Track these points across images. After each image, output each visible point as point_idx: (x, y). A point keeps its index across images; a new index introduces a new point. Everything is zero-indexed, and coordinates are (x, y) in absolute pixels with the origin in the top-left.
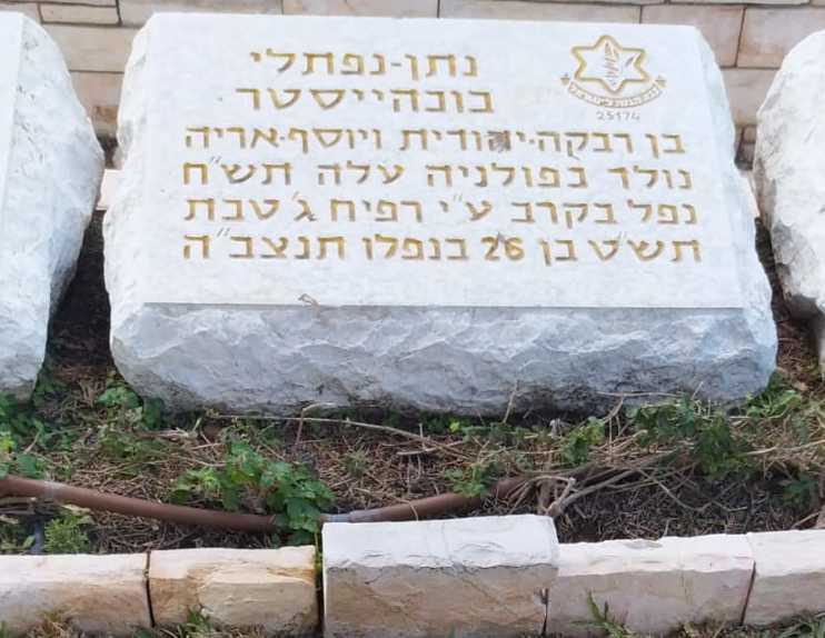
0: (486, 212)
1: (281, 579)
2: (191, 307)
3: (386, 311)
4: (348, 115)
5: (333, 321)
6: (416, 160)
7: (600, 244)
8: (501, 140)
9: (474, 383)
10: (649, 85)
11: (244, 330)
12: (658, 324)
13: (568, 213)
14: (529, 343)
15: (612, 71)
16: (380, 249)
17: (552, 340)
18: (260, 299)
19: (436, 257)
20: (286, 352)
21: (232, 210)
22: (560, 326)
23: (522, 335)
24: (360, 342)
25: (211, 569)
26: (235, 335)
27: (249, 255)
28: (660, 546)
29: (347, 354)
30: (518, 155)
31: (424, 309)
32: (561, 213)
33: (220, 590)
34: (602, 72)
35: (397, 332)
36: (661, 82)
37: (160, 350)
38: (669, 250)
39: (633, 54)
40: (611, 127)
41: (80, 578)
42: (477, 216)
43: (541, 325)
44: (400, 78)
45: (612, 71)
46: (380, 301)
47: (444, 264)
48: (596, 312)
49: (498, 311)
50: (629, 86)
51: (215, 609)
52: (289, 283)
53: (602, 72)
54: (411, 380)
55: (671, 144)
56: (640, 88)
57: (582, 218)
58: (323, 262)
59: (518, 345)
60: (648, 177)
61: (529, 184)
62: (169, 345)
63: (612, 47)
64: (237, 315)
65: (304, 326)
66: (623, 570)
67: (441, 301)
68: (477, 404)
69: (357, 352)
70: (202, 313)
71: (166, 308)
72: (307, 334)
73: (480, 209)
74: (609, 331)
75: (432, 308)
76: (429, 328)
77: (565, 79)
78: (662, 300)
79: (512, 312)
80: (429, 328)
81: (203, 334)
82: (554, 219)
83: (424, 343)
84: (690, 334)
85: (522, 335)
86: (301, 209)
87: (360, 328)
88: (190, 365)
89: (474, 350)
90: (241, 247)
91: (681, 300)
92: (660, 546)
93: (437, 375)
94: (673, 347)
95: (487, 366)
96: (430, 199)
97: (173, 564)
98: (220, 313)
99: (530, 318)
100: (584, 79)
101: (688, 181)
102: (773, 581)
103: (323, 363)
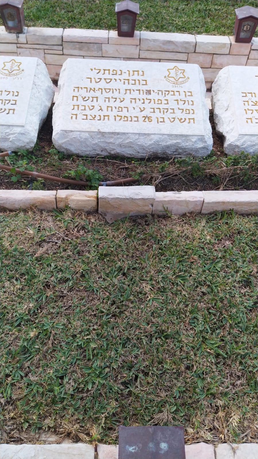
1: (88, 199)
2: (72, 131)
3: (118, 134)
4: (113, 85)
6: (128, 96)
8: (149, 92)
9: (139, 151)
11: (84, 137)
14: (152, 142)
23: (151, 140)
24: (112, 140)
25: (72, 195)
26: (82, 138)
29: (109, 143)
30: (153, 96)
31: (127, 133)
33: (73, 200)
34: (174, 75)
35: (121, 138)
42: (142, 111)
43: (155, 138)
44: (125, 76)
46: (117, 131)
48: (170, 135)
49: (145, 134)
50: (173, 78)
51: (72, 205)
53: (174, 75)
56: (17, 72)
59: (150, 143)
63: (177, 69)
64: (83, 133)
66: (171, 199)
67: (132, 131)
69: (111, 143)
71: (66, 131)
72: (99, 138)
74: (172, 140)
78: (185, 133)
79: (148, 135)
80: (128, 138)
81: (74, 138)
84: (191, 141)
86: (100, 108)
88: (71, 145)
90: (85, 117)
94: (187, 144)
95: (142, 147)
97: (63, 193)
98: (78, 133)
99: (153, 136)
102: (208, 203)
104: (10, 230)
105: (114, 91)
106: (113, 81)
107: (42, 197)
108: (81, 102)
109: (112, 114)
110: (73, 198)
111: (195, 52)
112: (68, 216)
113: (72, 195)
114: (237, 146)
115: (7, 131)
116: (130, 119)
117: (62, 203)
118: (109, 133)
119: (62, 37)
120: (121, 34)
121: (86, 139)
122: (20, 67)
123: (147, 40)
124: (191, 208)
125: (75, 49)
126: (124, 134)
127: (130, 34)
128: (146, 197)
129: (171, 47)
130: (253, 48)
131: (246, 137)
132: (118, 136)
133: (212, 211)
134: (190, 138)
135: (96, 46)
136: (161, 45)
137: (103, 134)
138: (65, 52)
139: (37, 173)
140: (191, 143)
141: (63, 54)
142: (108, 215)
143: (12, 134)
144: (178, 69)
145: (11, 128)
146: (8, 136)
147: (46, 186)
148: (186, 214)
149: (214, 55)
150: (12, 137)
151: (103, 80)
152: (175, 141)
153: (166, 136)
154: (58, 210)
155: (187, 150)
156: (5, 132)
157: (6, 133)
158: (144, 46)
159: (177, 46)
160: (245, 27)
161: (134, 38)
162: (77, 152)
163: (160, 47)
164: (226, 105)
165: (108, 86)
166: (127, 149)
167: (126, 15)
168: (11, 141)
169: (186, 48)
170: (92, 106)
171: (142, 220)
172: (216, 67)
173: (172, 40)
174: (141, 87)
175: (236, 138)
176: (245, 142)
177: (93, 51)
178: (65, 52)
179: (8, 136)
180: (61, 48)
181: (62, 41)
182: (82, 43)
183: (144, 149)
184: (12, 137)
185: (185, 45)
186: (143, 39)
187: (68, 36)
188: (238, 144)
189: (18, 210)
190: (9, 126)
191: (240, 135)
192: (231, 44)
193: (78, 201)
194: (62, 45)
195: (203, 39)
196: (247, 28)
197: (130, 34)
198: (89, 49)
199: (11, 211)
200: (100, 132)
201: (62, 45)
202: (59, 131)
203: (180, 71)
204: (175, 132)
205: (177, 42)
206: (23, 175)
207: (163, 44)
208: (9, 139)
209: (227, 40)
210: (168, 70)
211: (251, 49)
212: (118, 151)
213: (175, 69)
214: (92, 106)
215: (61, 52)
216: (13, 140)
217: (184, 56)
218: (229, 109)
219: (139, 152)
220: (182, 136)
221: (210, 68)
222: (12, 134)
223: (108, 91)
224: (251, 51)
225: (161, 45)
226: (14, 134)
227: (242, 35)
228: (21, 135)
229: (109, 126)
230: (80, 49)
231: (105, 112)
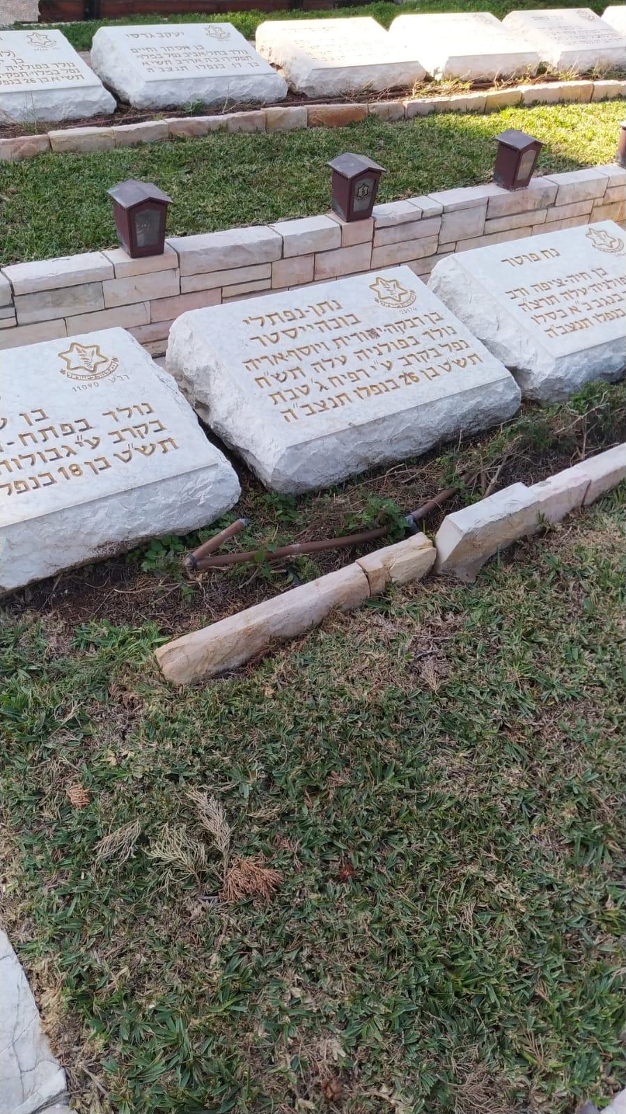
0: (98, 443)
1: (423, 551)
2: (306, 443)
3: (384, 419)
4: (304, 339)
5: (365, 430)
6: (348, 351)
7: (121, 455)
8: (373, 333)
9: (422, 440)
10: (109, 363)
11: (331, 447)
12: (483, 393)
14: (442, 414)
15: (86, 361)
16: (363, 393)
17: (450, 411)
18: (333, 430)
19: (37, 487)
20: (347, 451)
21: (290, 395)
22: (451, 404)
23: (438, 413)
24: (375, 437)
25: (390, 558)
26: (328, 450)
27: (314, 412)
28: (550, 482)
29: (369, 444)
30: (384, 337)
31: (398, 413)
32: (13, 465)
33: (400, 566)
35: (389, 427)
36: (115, 359)
37: (296, 468)
38: (159, 448)
39: (92, 349)
40: (410, 316)
41: (341, 584)
42: (389, 368)
43: (445, 406)
44: (312, 318)
45: (86, 361)
46: (381, 415)
47: (42, 490)
48: (463, 394)
49: (426, 405)
51: (399, 577)
52: (341, 418)
54: (396, 447)
55: (38, 415)
57: (146, 432)
58: (345, 406)
59: (438, 417)
60: (127, 412)
61: (57, 436)
62: (299, 464)
64: (327, 441)
65: (353, 437)
66: (549, 496)
67: (403, 408)
68: (204, 524)
69: (375, 442)
70: (312, 444)
71: (296, 447)
72: (355, 440)
73: (95, 442)
74: (467, 401)
75: (402, 412)
76: (402, 421)
78: (482, 382)
79: (431, 404)
80: (402, 421)
81: (314, 454)
83: (402, 429)
84: (496, 392)
85: (438, 413)
86: (319, 386)
87: (375, 430)
88: (307, 471)
89: (422, 425)
90: (308, 410)
91: (488, 380)
92: (550, 482)
93: (406, 441)
94: (492, 400)
95: (427, 431)
96: (366, 364)
97: (374, 560)
98: (319, 442)
99: (439, 404)
101: (149, 408)
102: (598, 481)
103: (362, 452)
104: (339, 671)
105: (317, 347)
106: (300, 331)
107: (347, 583)
108: (276, 386)
109: (348, 387)
110: (397, 561)
111: (282, 258)
112: (399, 602)
113: (390, 558)
114: (560, 380)
115: (189, 485)
117: (380, 580)
118: (370, 423)
119: (12, 286)
120: (136, 253)
121: (335, 449)
122: (101, 352)
123: (192, 253)
124: (575, 501)
125: (45, 306)
126: (393, 415)
127: (156, 249)
128: (529, 504)
129: (239, 259)
130: (377, 226)
131: (567, 360)
132: (385, 424)
133: (597, 495)
134: (493, 387)
135: (90, 290)
136: (222, 258)
137: (357, 429)
138: (22, 318)
139: (421, 510)
140: (497, 397)
141: (17, 325)
142: (457, 571)
143: (201, 489)
145: (193, 476)
146: (192, 496)
147: (329, 563)
148: (568, 515)
149: (317, 255)
150: (202, 497)
151: (282, 336)
152: (473, 402)
153: (458, 397)
154: (378, 598)
155: (492, 412)
156: (185, 489)
157: (188, 491)
158: (188, 267)
159: (250, 252)
160: (360, 190)
161: (164, 255)
162: (319, 483)
163: (220, 262)
164: (494, 321)
165: (299, 343)
166: (401, 444)
167: (147, 211)
168: (202, 506)
169: (266, 253)
171: (522, 548)
172: (324, 276)
173: (240, 243)
174: (353, 329)
175: (554, 367)
176: (568, 368)
177: (86, 301)
178: (22, 318)
179: (192, 496)
180: (11, 311)
181: (13, 295)
182: (57, 289)
183: (429, 434)
184: (202, 497)
185: (265, 248)
186: (184, 253)
187: (26, 280)
188: (560, 374)
189: (308, 631)
190: (188, 474)
191: (557, 359)
192: (341, 227)
193: (409, 562)
194: (13, 305)
195: (286, 228)
196: (363, 192)
197: (156, 249)
198: (76, 299)
199: (297, 638)
200: (355, 427)
201: (13, 305)
202: (283, 452)
204: (467, 386)
205: (249, 245)
206: (272, 560)
207: (225, 255)
208: (198, 500)
209: (326, 222)
211: (375, 229)
212: (387, 454)
215: (13, 322)
216: (208, 499)
217: (452, 247)
218: (501, 325)
219: (420, 443)
220: (481, 388)
221: (314, 281)
222: (201, 489)
223: (306, 351)
224: (377, 232)
225: (222, 258)
226: (206, 486)
227: (357, 205)
228: (218, 485)
229: (363, 411)
230: (57, 304)
231: (333, 392)
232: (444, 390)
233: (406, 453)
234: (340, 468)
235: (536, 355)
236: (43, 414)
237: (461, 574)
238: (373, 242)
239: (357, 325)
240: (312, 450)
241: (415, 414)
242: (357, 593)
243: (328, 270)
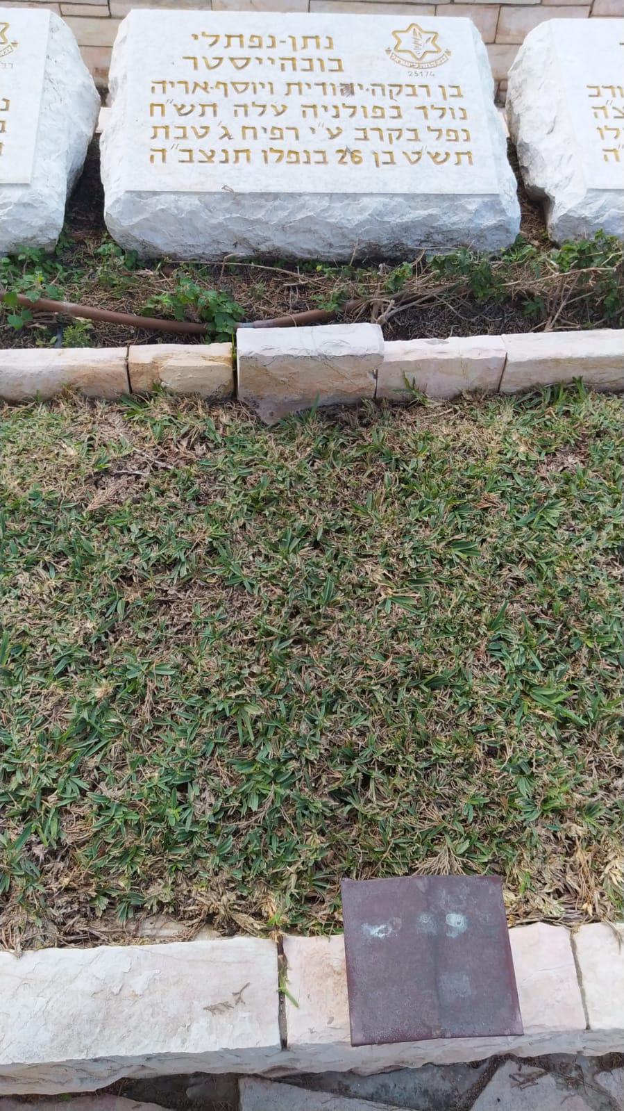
2: (155, 193)
3: (276, 196)
4: (253, 73)
6: (295, 101)
8: (348, 89)
9: (332, 241)
11: (188, 208)
12: (446, 204)
13: (390, 135)
14: (366, 215)
17: (380, 214)
18: (198, 188)
20: (214, 221)
21: (180, 133)
22: (385, 205)
23: (361, 211)
24: (260, 215)
25: (167, 357)
26: (182, 211)
27: (191, 161)
29: (253, 223)
31: (300, 195)
33: (173, 370)
34: (411, 47)
35: (283, 209)
37: (136, 220)
39: (428, 36)
40: (416, 81)
41: (85, 363)
42: (333, 137)
43: (373, 204)
44: (285, 50)
46: (273, 189)
51: (169, 382)
52: (216, 178)
53: (411, 47)
58: (237, 165)
62: (141, 217)
63: (418, 31)
64: (184, 198)
65: (225, 205)
67: (311, 189)
69: (258, 221)
70: (163, 197)
71: (139, 194)
72: (227, 210)
74: (416, 209)
77: (388, 51)
78: (448, 189)
79: (355, 197)
81: (162, 210)
82: (381, 138)
83: (300, 216)
84: (466, 210)
85: (361, 211)
86: (223, 132)
87: (261, 207)
89: (332, 220)
90: (186, 156)
93: (309, 236)
94: (456, 219)
95: (339, 230)
97: (143, 354)
98: (172, 197)
99: (366, 200)
100: (400, 51)
102: (518, 364)
103: (238, 228)
104: (15, 450)
105: (259, 87)
113: (167, 357)
114: (584, 220)
116: (303, 157)
118: (254, 195)
121: (193, 212)
128: (361, 353)
131: (606, 196)
134: (463, 201)
137: (236, 198)
140: (466, 217)
141: (110, 17)
142: (262, 405)
144: (420, 29)
149: (504, 9)
152: (424, 213)
153: (400, 199)
154: (134, 396)
165: (241, 76)
170: (203, 128)
171: (352, 414)
172: (508, 39)
175: (580, 200)
176: (602, 208)
188: (586, 213)
202: (121, 195)
203: (426, 36)
204: (422, 189)
210: (394, 33)
212: (278, 244)
213: (411, 32)
214: (203, 128)
215: (104, 11)
219: (331, 245)
220: (442, 197)
228: (22, 209)
229: (250, 177)
232: (385, 184)
233: (310, 252)
234: (202, 240)
235: (569, 179)
236: (324, 158)
237: (264, 413)
238: (592, 6)
239: (457, 99)
240: (165, 202)
241: (325, 203)
242: (105, 381)
243: (513, 32)
